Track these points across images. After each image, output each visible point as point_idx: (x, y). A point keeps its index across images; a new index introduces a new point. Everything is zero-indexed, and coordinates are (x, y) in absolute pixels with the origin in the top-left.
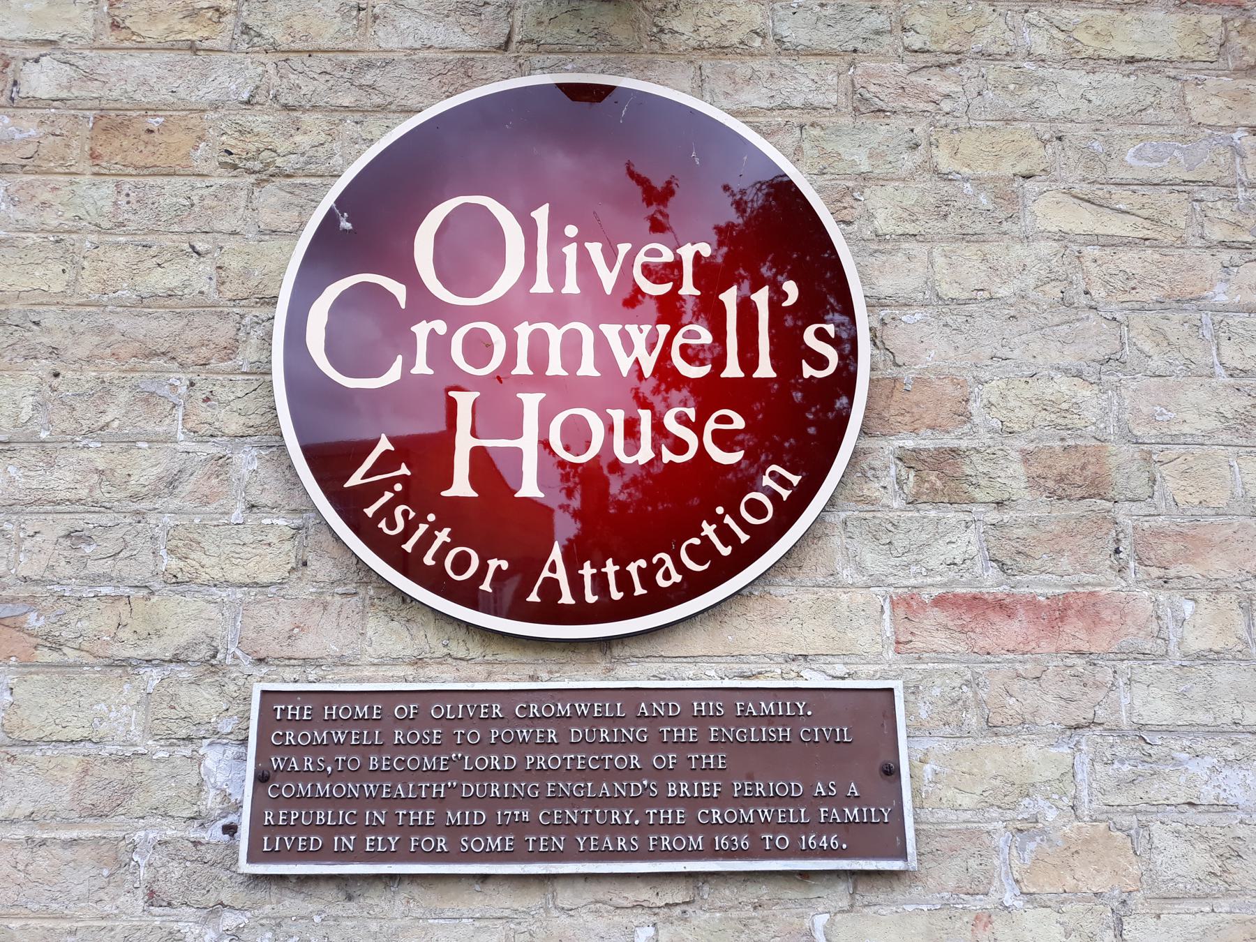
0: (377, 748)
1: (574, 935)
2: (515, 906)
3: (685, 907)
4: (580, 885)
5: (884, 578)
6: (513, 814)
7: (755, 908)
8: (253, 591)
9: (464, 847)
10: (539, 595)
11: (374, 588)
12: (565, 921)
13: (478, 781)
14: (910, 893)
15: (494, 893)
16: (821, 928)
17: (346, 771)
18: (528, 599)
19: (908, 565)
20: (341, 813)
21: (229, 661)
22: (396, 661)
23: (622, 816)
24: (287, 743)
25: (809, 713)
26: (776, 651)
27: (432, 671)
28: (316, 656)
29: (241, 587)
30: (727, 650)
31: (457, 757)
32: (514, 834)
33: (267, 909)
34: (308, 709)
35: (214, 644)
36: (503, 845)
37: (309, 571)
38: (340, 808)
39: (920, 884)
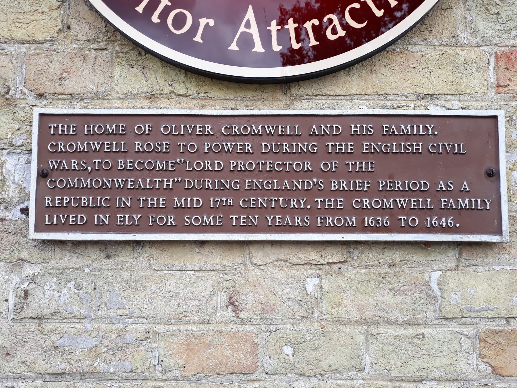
0: (123, 154)
1: (264, 282)
2: (224, 262)
3: (340, 265)
4: (268, 249)
5: (491, 39)
6: (222, 201)
7: (390, 267)
8: (33, 47)
9: (187, 222)
10: (237, 45)
11: (118, 45)
12: (257, 272)
13: (196, 178)
14: (499, 258)
15: (209, 254)
16: (436, 281)
17: (101, 170)
18: (229, 48)
19: (510, 30)
20: (99, 198)
21: (18, 96)
22: (136, 96)
23: (299, 202)
24: (59, 150)
25: (436, 133)
26: (411, 91)
27: (161, 103)
28: (79, 92)
29: (23, 43)
30: (375, 90)
31: (180, 161)
32: (222, 213)
33: (53, 263)
34: (73, 127)
35: (7, 84)
36: (215, 221)
37: (72, 32)
38: (99, 196)
39: (506, 252)
